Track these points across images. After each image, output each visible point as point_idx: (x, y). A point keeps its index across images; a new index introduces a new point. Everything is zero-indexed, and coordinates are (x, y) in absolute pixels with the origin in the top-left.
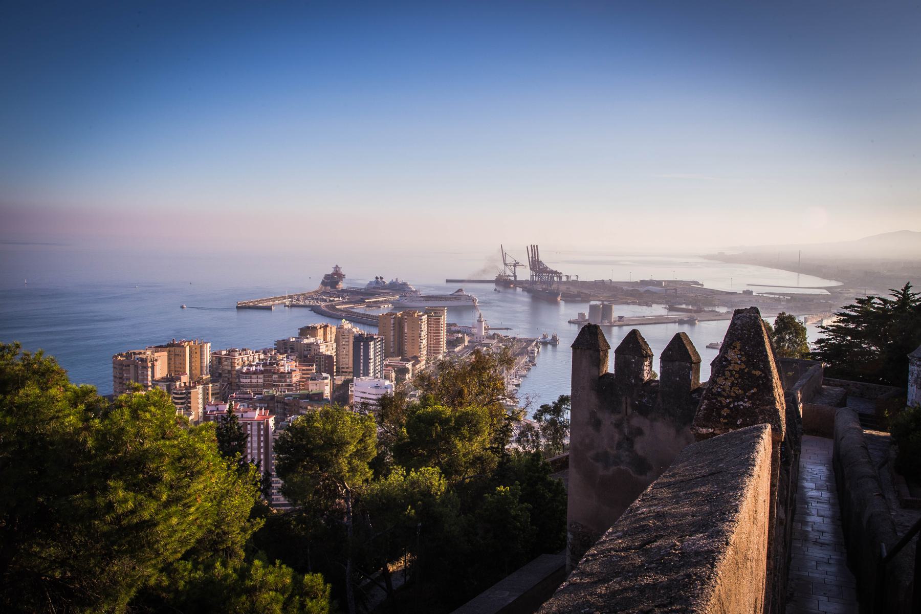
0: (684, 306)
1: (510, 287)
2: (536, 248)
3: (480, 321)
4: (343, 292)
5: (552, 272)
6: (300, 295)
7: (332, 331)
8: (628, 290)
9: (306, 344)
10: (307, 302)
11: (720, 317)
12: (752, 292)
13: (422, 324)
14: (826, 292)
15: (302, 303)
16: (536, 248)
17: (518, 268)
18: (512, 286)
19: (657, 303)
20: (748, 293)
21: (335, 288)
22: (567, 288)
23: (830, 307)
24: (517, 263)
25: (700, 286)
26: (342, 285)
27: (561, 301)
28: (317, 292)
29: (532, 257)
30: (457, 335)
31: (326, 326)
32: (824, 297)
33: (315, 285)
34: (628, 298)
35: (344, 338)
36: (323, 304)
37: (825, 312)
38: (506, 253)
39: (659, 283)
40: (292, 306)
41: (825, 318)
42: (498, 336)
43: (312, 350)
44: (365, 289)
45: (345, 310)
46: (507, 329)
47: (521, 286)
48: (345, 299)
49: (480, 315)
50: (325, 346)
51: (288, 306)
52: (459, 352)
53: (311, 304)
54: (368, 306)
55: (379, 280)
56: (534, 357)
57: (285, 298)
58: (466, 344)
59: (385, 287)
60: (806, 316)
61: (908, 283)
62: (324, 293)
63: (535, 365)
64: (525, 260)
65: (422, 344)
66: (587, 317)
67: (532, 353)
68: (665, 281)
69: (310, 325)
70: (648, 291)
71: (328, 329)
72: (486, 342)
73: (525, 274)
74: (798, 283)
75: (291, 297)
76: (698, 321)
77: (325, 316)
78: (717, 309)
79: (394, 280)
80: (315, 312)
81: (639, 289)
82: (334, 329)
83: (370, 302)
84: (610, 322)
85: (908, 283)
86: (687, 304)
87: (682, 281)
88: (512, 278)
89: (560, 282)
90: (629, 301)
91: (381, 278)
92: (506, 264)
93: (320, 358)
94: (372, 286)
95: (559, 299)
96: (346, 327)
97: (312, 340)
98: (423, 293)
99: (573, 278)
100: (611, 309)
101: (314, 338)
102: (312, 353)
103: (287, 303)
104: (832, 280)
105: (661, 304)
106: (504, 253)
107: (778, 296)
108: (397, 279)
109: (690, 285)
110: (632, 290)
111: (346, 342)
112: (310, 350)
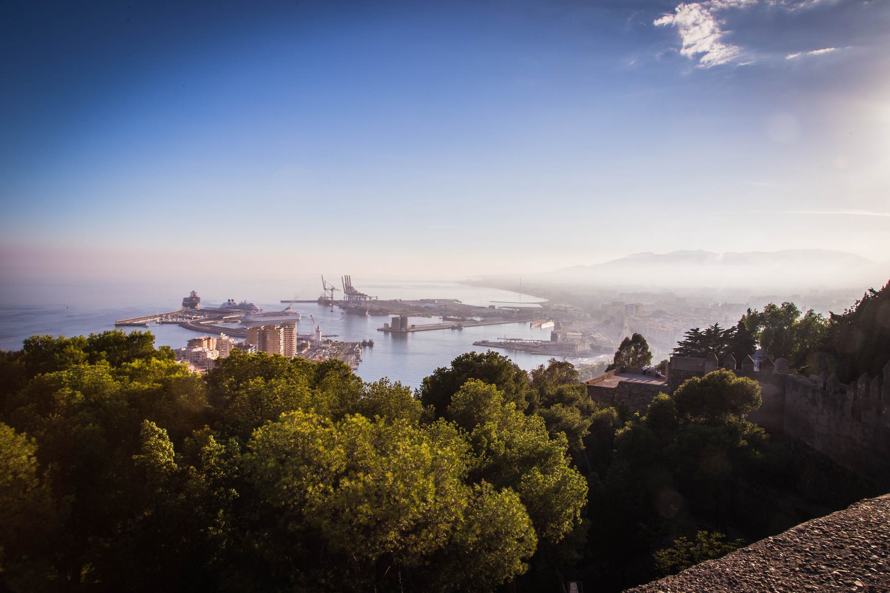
0: (452, 317)
1: (329, 305)
2: (348, 278)
3: (318, 331)
4: (202, 312)
5: (360, 294)
6: (168, 314)
7: (214, 341)
8: (413, 306)
9: (195, 352)
10: (175, 320)
13: (281, 335)
14: (539, 306)
15: (170, 320)
16: (348, 278)
17: (334, 292)
18: (330, 304)
21: (195, 308)
26: (199, 306)
28: (181, 312)
29: (346, 284)
31: (209, 339)
32: (539, 309)
33: (179, 307)
35: (222, 347)
36: (189, 321)
39: (433, 301)
40: (163, 323)
41: (543, 323)
42: (331, 341)
43: (201, 357)
44: (219, 309)
45: (208, 325)
46: (335, 336)
48: (205, 316)
49: (318, 327)
50: (211, 353)
51: (159, 323)
52: (306, 353)
53: (178, 321)
54: (225, 322)
55: (231, 302)
57: (156, 316)
59: (235, 307)
60: (531, 322)
62: (186, 312)
63: (361, 361)
64: (340, 286)
65: (281, 349)
66: (390, 326)
68: (437, 300)
69: (197, 338)
70: (426, 307)
71: (211, 340)
73: (340, 295)
75: (161, 316)
77: (193, 330)
78: (474, 318)
79: (243, 302)
80: (183, 327)
81: (421, 306)
82: (215, 340)
83: (227, 319)
84: (406, 329)
86: (454, 316)
88: (330, 299)
89: (366, 302)
90: (416, 314)
91: (233, 300)
92: (325, 289)
93: (208, 362)
94: (226, 306)
95: (367, 313)
96: (224, 338)
97: (199, 349)
98: (265, 311)
99: (373, 299)
100: (407, 320)
101: (201, 348)
102: (201, 359)
103: (158, 321)
108: (245, 301)
110: (416, 307)
111: (224, 349)
112: (199, 357)
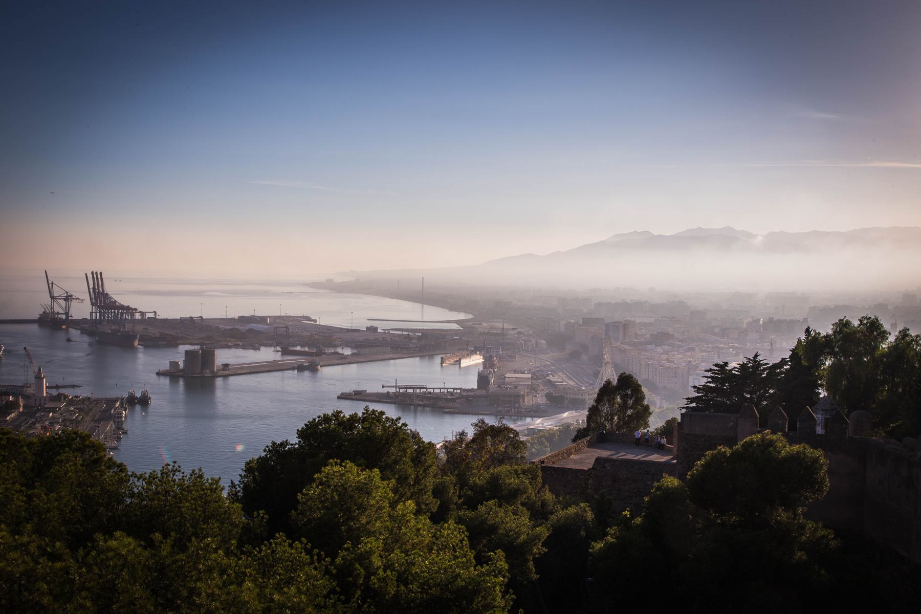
0: (298, 348)
1: (61, 329)
5: (122, 307)
11: (344, 361)
12: (376, 328)
14: (455, 326)
18: (64, 327)
19: (266, 345)
20: (372, 329)
22: (145, 329)
23: (467, 345)
24: (69, 296)
25: (313, 323)
27: (139, 347)
29: (94, 288)
30: (7, 398)
32: (456, 332)
34: (227, 339)
37: (463, 349)
38: (52, 283)
39: (263, 320)
41: (464, 357)
47: (78, 327)
56: (122, 421)
58: (21, 410)
60: (443, 356)
61: (757, 353)
64: (81, 291)
67: (118, 417)
68: (270, 317)
72: (50, 406)
73: (83, 310)
74: (422, 317)
76: (321, 366)
78: (340, 350)
84: (212, 372)
85: (757, 353)
86: (302, 346)
87: (290, 317)
88: (64, 317)
89: (133, 321)
90: (230, 344)
92: (53, 298)
95: (136, 343)
104: (461, 312)
105: (270, 346)
106: (50, 282)
107: (407, 333)
109: (300, 321)
110: (230, 330)
